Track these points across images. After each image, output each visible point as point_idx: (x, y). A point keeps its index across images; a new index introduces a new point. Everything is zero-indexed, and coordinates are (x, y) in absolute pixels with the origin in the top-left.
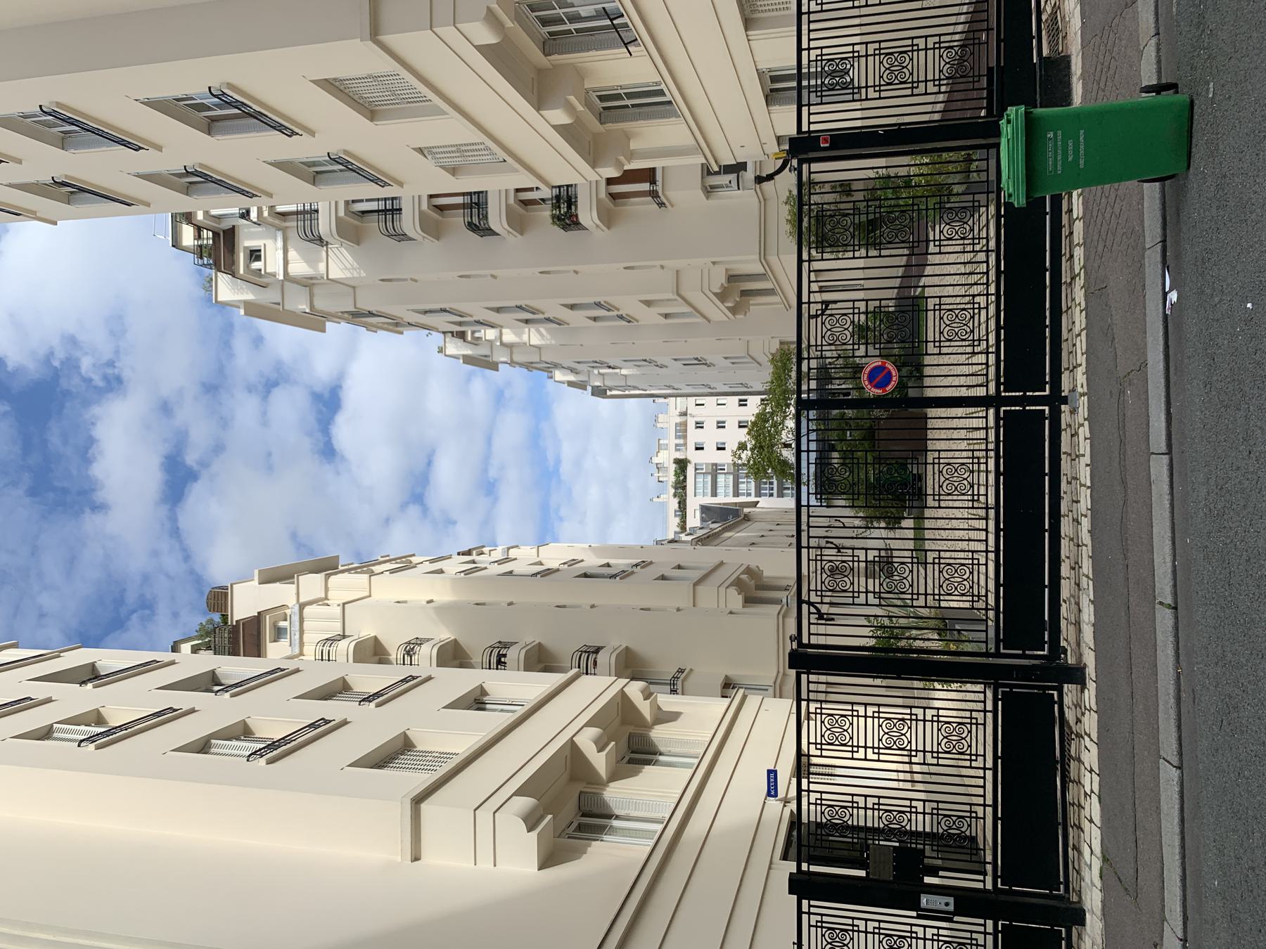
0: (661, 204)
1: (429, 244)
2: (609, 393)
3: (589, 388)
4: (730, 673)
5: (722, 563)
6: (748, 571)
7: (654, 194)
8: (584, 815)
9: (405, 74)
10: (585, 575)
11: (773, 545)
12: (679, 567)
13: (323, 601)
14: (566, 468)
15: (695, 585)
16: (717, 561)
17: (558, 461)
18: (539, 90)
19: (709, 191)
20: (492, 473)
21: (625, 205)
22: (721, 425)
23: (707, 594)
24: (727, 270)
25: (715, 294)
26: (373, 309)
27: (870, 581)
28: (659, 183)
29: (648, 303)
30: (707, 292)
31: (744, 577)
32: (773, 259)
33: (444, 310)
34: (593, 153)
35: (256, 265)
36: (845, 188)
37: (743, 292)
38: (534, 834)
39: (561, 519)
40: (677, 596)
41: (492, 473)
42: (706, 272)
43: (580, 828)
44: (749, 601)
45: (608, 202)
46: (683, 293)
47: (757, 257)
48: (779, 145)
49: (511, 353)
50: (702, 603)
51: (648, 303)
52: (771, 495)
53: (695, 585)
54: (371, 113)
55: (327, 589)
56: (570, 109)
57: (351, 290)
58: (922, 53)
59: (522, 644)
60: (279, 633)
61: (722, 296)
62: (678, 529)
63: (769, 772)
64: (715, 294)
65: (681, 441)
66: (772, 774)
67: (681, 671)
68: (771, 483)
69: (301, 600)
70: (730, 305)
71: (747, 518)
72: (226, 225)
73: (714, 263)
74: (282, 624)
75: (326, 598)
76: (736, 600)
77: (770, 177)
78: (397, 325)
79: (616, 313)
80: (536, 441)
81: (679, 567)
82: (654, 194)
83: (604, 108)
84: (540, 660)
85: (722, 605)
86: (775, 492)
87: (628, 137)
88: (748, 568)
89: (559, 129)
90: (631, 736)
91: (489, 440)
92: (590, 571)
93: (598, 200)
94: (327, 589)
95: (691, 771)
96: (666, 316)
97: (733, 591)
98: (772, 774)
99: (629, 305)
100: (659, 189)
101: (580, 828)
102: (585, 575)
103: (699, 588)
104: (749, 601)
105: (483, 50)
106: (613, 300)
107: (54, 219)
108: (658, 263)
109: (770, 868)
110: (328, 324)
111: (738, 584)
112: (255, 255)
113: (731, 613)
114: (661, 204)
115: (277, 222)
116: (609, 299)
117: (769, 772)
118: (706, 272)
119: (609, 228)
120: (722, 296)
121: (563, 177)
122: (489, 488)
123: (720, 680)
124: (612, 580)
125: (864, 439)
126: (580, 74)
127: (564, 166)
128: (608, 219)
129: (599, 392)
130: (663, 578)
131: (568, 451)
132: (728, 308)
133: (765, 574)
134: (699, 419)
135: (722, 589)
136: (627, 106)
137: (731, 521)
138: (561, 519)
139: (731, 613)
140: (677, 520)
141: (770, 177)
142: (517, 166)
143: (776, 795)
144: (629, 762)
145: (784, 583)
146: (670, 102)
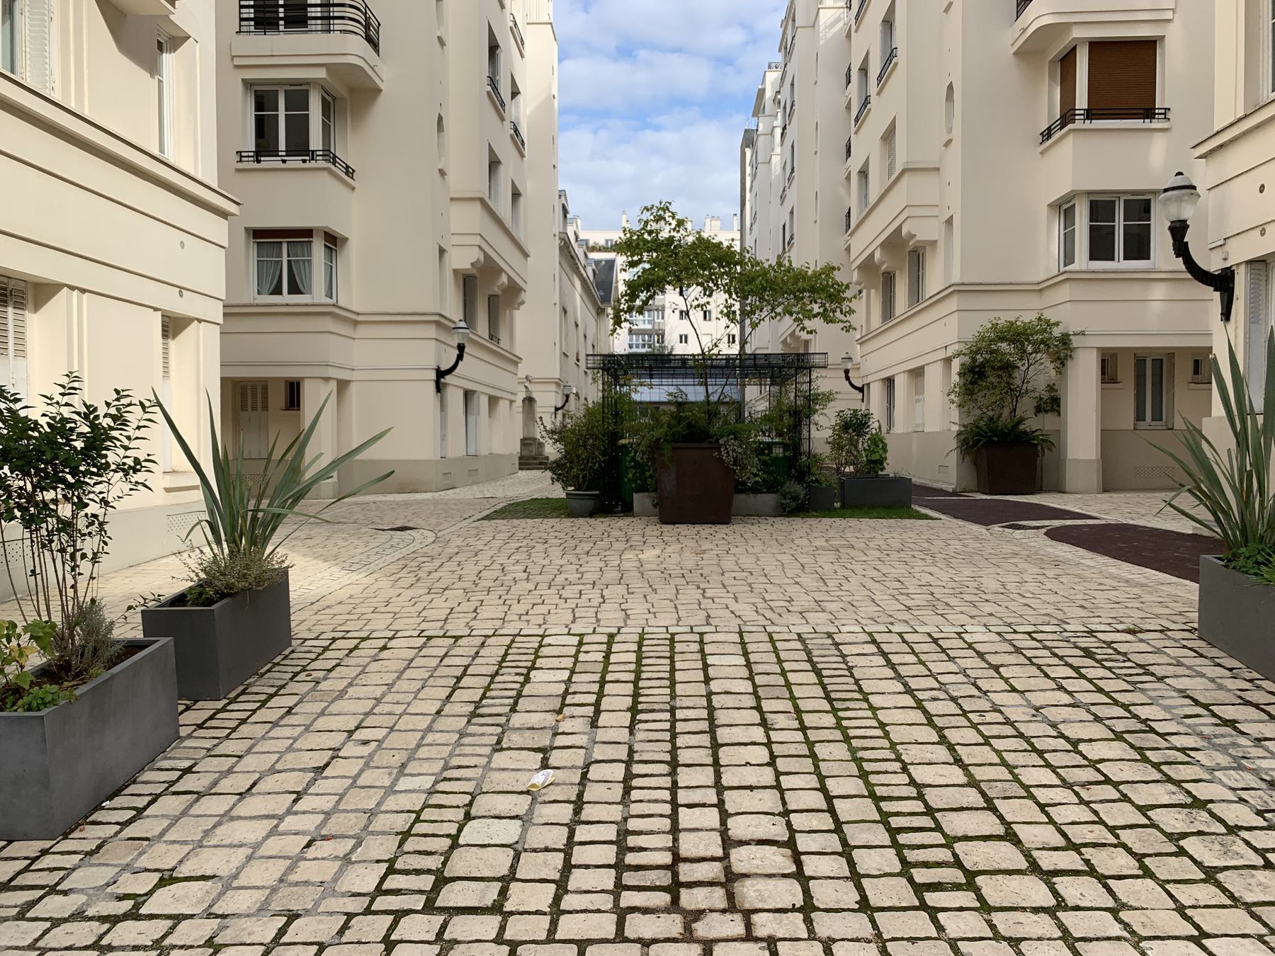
0: (1047, 134)
5: (526, 255)
7: (1067, 116)
10: (494, 48)
11: (564, 336)
12: (516, 195)
14: (649, 136)
15: (482, 201)
16: (529, 248)
17: (657, 128)
19: (1064, 207)
20: (643, 54)
21: (1051, 78)
23: (468, 219)
25: (899, 228)
28: (1088, 124)
31: (504, 279)
32: (953, 304)
36: (1052, 404)
39: (595, 132)
40: (467, 174)
41: (643, 54)
42: (935, 212)
46: (905, 179)
47: (956, 279)
50: (457, 211)
52: (631, 346)
53: (482, 201)
62: (591, 244)
64: (899, 228)
67: (349, 171)
68: (644, 346)
70: (877, 256)
71: (600, 312)
73: (949, 222)
76: (463, 259)
77: (848, 378)
80: (677, 103)
81: (516, 195)
85: (455, 240)
87: (876, 289)
88: (520, 290)
89: (872, 254)
91: (677, 50)
92: (502, 55)
93: (1067, 26)
97: (475, 255)
100: (1078, 124)
102: (494, 48)
103: (478, 205)
104: (468, 283)
106: (898, 79)
108: (957, 135)
113: (442, 251)
118: (935, 212)
119: (1015, 54)
120: (895, 242)
122: (626, 51)
123: (338, 228)
124: (487, 81)
125: (80, 607)
126: (901, 269)
128: (1028, 52)
131: (669, 139)
132: (872, 254)
133: (516, 312)
135: (477, 240)
137: (597, 294)
138: (595, 132)
139: (442, 251)
140: (602, 243)
141: (848, 378)
145: (503, 335)
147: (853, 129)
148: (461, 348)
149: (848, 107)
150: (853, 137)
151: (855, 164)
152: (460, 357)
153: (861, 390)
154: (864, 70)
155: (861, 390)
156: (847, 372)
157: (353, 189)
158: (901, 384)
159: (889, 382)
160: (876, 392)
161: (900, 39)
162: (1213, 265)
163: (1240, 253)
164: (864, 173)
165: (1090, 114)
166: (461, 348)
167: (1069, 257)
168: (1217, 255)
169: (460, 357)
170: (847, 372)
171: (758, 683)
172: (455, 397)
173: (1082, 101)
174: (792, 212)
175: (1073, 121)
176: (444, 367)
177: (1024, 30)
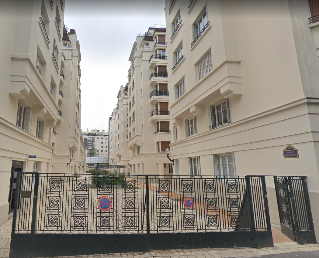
0: (155, 133)
1: (149, 83)
2: (110, 121)
3: (112, 117)
4: (55, 145)
6: (76, 148)
7: (158, 131)
8: (24, 108)
9: (211, 71)
13: (72, 56)
18: (200, 106)
22: (102, 143)
24: (141, 146)
26: (135, 70)
27: (88, 184)
29: (134, 129)
30: (137, 142)
33: (134, 85)
34: (178, 119)
35: (145, 45)
37: (135, 149)
38: (19, 93)
43: (21, 107)
44: (71, 149)
45: (157, 122)
48: (176, 159)
49: (121, 101)
51: (134, 129)
54: (198, 64)
55: (75, 56)
56: (194, 112)
57: (139, 66)
58: (208, 196)
59: (62, 99)
60: (65, 45)
61: (135, 145)
63: (36, 156)
64: (135, 143)
65: (99, 135)
66: (35, 157)
67: (56, 134)
69: (72, 51)
72: (154, 39)
73: (143, 143)
74: (67, 46)
75: (73, 56)
77: (168, 157)
78: (130, 76)
79: (132, 122)
81: (77, 134)
82: (158, 131)
83: (189, 121)
84: (60, 102)
86: (89, 153)
90: (44, 122)
94: (75, 56)
95: (48, 143)
96: (130, 133)
97: (73, 145)
98: (35, 157)
99: (133, 125)
100: (159, 132)
101: (21, 107)
104: (71, 149)
105: (219, 90)
107: (24, 128)
109: (10, 157)
110: (130, 61)
111: (74, 146)
112: (147, 44)
114: (155, 133)
115: (155, 50)
116: (135, 121)
117: (36, 156)
119: (151, 122)
120: (135, 145)
121: (171, 112)
127: (174, 112)
128: (153, 122)
129: (110, 119)
130: (76, 130)
134: (103, 139)
136: (189, 125)
141: (168, 157)
142: (176, 101)
143: (30, 158)
144: (38, 121)
146: (189, 136)
147: (128, 112)
148: (71, 160)
149: (127, 109)
150: (128, 113)
151: (128, 117)
152: (71, 162)
153: (130, 165)
154: (130, 103)
155: (130, 165)
156: (128, 162)
157: (56, 136)
158: (136, 165)
159: (134, 165)
160: (132, 166)
161: (135, 100)
162: (172, 159)
163: (175, 158)
164: (130, 118)
165: (161, 131)
166: (71, 160)
167: (159, 151)
168: (172, 158)
169: (71, 162)
170: (128, 162)
171: (31, 177)
172: (68, 166)
173: (159, 129)
174: (118, 124)
175: (159, 132)
176: (68, 163)
177: (152, 119)
